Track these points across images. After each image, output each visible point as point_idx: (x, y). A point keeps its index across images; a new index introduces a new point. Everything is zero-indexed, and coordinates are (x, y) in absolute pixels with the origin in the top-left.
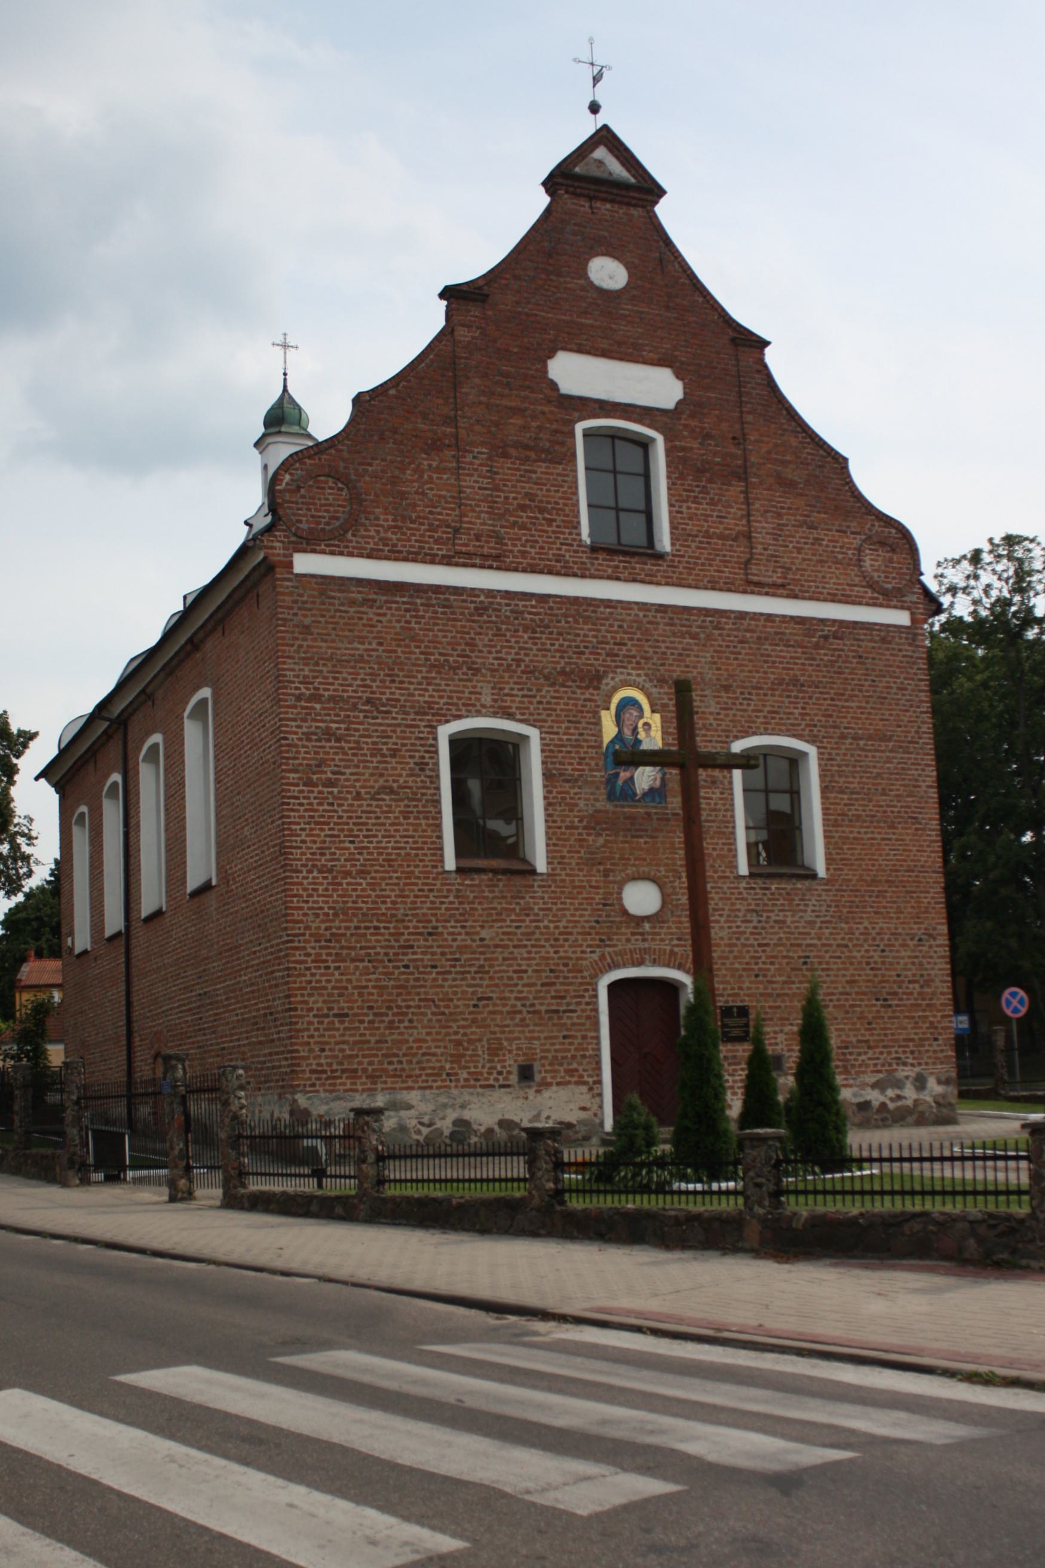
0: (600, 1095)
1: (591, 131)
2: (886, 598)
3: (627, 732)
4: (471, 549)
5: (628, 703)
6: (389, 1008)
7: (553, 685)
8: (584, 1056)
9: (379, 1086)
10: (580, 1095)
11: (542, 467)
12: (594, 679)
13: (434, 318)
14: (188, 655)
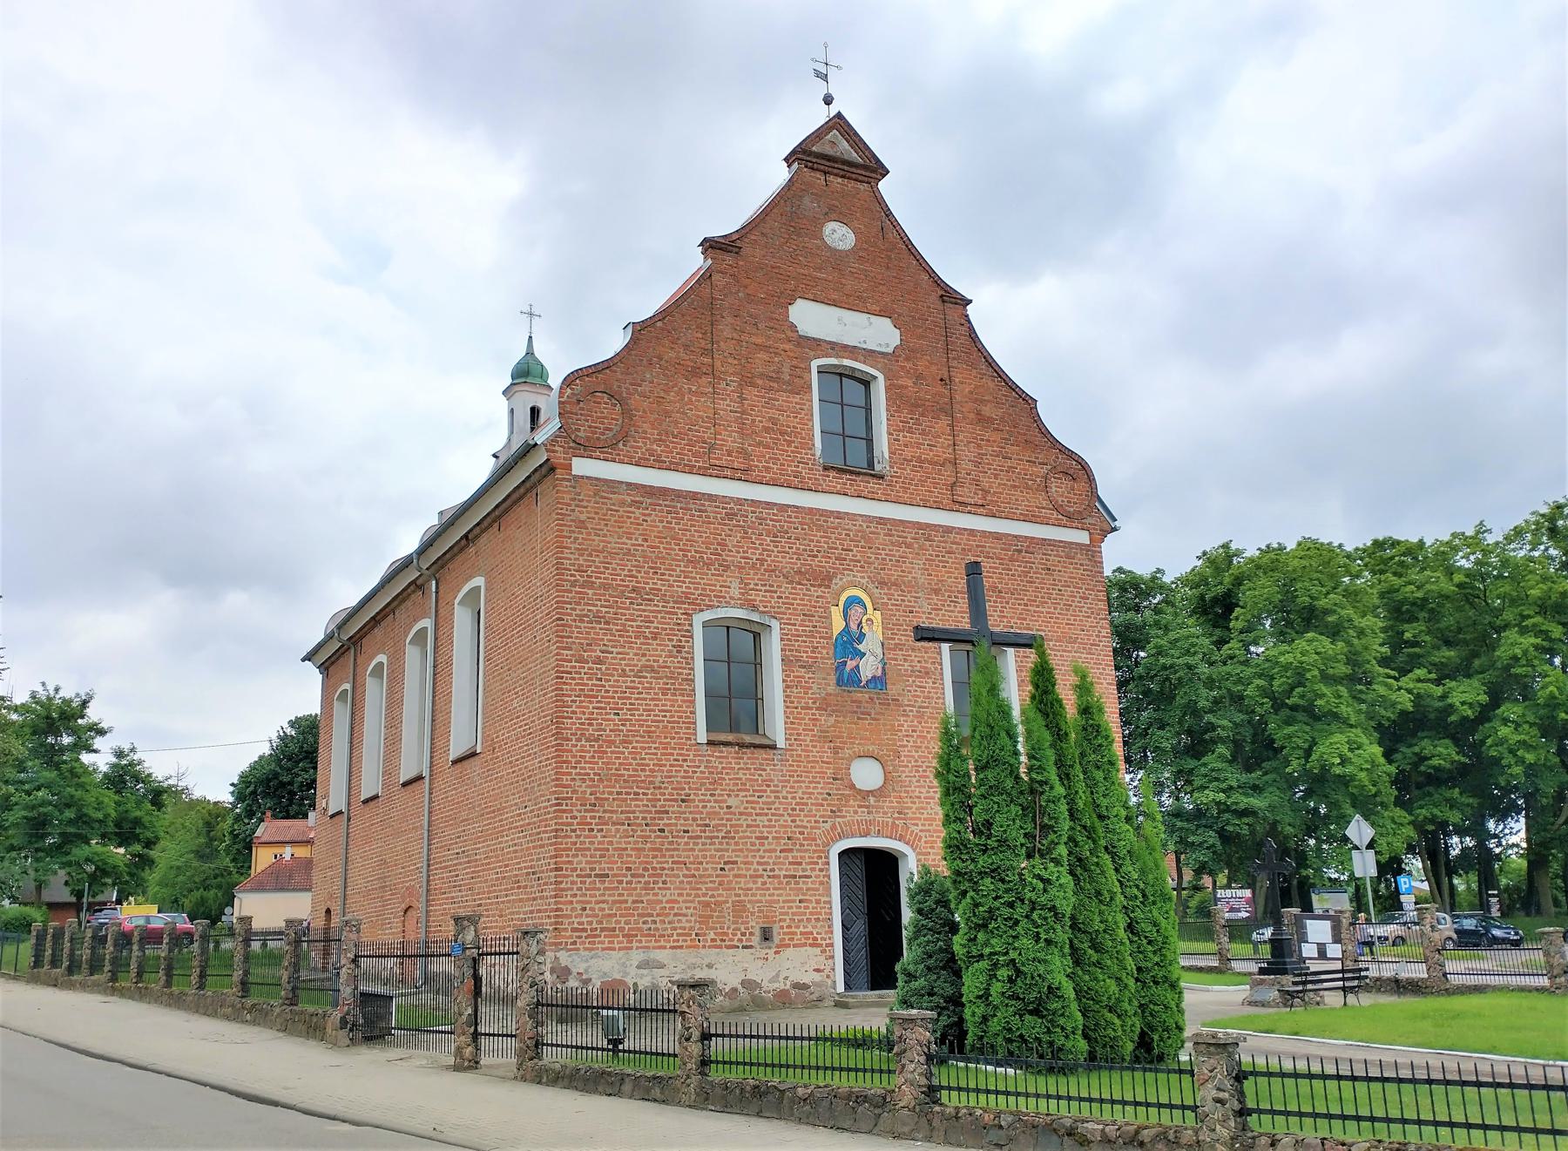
0: (832, 957)
1: (821, 120)
2: (1071, 519)
3: (853, 626)
4: (724, 463)
5: (853, 601)
6: (645, 869)
7: (791, 582)
8: (817, 920)
9: (635, 944)
10: (812, 956)
11: (783, 396)
12: (825, 580)
13: (696, 261)
14: (462, 550)
